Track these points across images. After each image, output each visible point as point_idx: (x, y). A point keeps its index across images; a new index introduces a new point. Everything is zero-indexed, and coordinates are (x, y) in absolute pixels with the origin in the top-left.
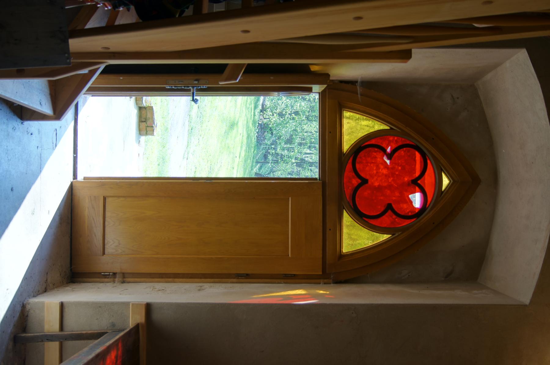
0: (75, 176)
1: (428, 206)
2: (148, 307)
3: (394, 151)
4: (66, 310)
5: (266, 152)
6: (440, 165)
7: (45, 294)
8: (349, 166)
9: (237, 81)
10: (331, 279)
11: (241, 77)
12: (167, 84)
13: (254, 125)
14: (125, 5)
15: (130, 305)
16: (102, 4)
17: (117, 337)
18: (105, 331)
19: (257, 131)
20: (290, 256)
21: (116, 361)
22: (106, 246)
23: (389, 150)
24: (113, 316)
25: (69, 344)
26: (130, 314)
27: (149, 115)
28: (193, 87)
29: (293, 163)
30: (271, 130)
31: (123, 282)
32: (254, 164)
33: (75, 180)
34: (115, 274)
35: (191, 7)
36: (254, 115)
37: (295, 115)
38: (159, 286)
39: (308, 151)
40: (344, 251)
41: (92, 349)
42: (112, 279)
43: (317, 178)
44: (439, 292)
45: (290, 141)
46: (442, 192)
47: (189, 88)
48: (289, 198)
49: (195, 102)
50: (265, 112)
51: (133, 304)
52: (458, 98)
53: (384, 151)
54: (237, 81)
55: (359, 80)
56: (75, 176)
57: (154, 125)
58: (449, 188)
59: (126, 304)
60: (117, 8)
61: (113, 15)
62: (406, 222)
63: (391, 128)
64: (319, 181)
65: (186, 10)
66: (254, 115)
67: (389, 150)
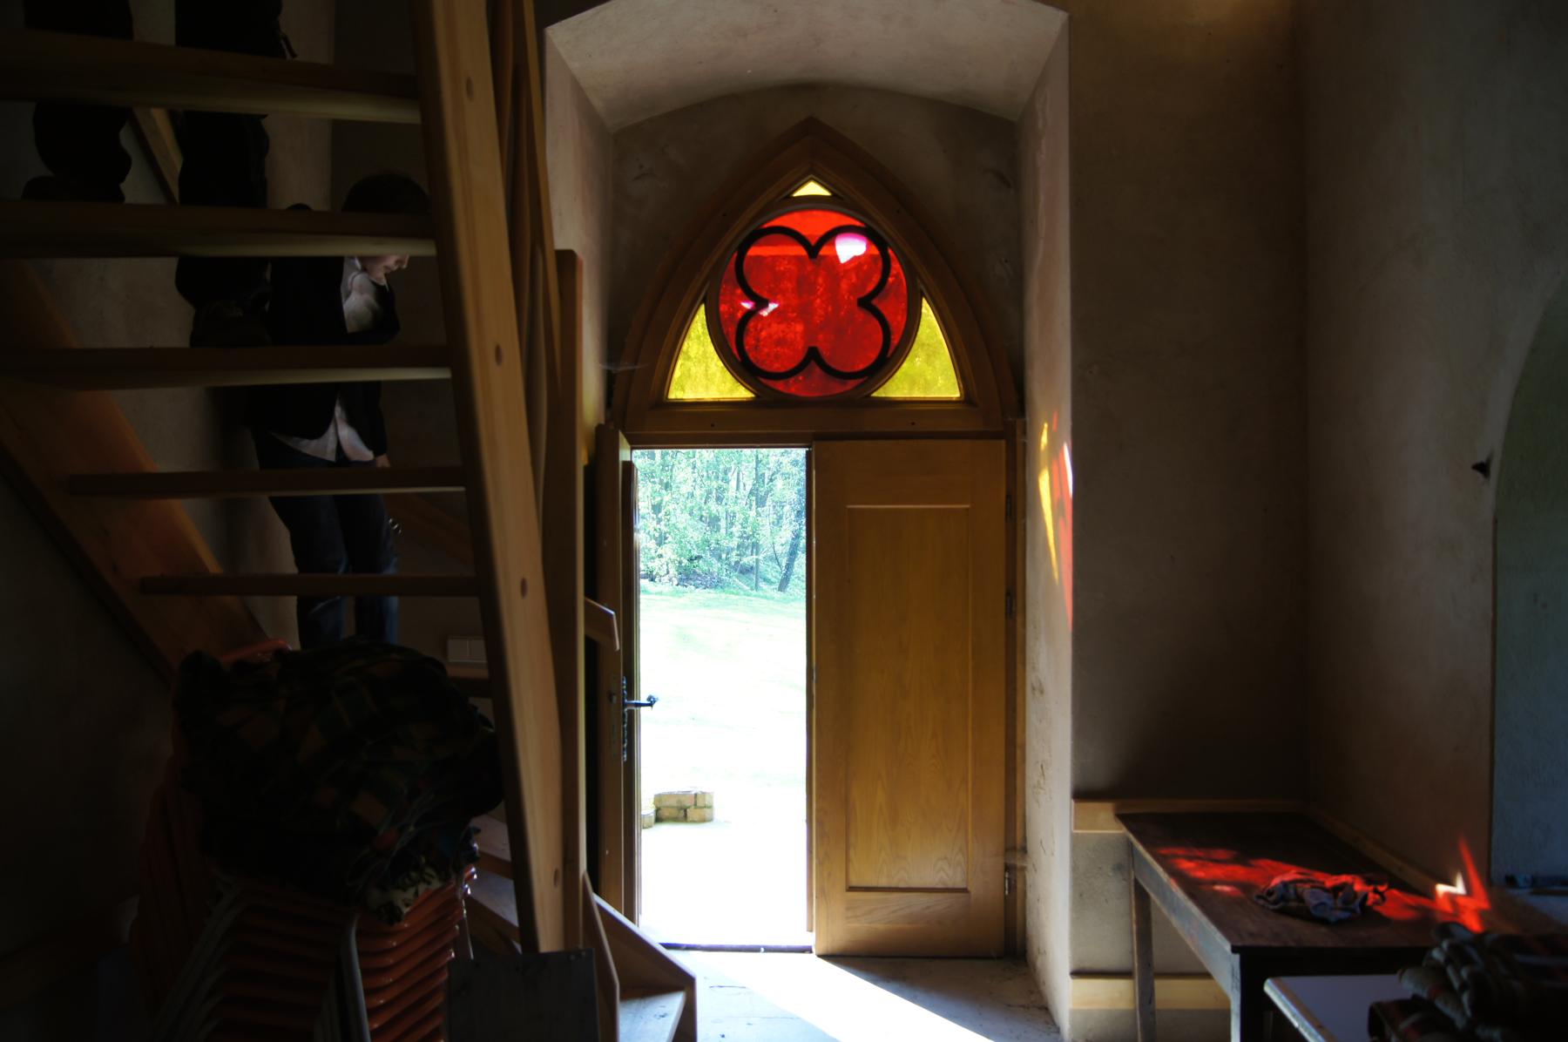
0: (807, 950)
1: (866, 224)
2: (1082, 794)
3: (751, 296)
4: (1088, 965)
5: (736, 570)
6: (781, 197)
7: (1053, 1009)
8: (779, 386)
9: (613, 613)
10: (1015, 422)
11: (603, 605)
12: (619, 760)
13: (681, 595)
14: (468, 838)
15: (1077, 834)
16: (467, 886)
17: (1148, 857)
18: (1133, 883)
19: (693, 587)
20: (968, 506)
21: (1198, 858)
22: (950, 885)
23: (747, 305)
24: (1100, 868)
25: (1159, 956)
26: (1095, 834)
27: (673, 802)
28: (625, 705)
29: (758, 514)
30: (691, 560)
31: (1024, 850)
32: (761, 593)
33: (814, 950)
34: (1008, 868)
35: (473, 701)
36: (661, 593)
37: (660, 512)
38: (1032, 774)
39: (733, 483)
40: (958, 395)
41: (1175, 908)
42: (1018, 874)
43: (807, 452)
44: (1042, 198)
45: (713, 522)
46: (834, 195)
47: (626, 714)
48: (849, 509)
49: (655, 702)
50: (654, 573)
51: (1076, 828)
52: (641, 167)
53: (749, 314)
54: (613, 613)
55: (606, 367)
56: (807, 950)
57: (693, 793)
58: (826, 181)
59: (1076, 842)
60: (475, 853)
61: (490, 864)
62: (896, 267)
63: (704, 301)
64: (814, 446)
65: (479, 711)
66: (661, 593)
67: (747, 305)
